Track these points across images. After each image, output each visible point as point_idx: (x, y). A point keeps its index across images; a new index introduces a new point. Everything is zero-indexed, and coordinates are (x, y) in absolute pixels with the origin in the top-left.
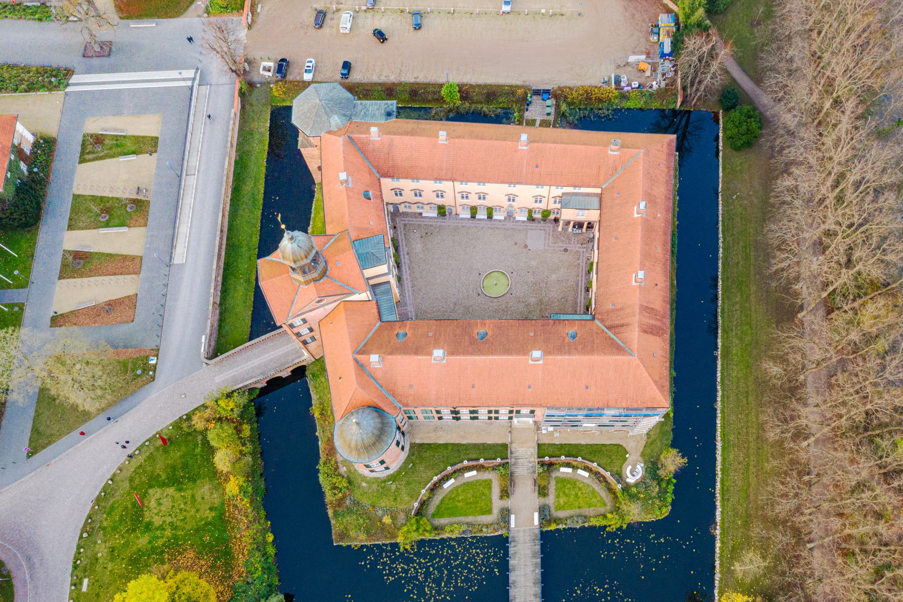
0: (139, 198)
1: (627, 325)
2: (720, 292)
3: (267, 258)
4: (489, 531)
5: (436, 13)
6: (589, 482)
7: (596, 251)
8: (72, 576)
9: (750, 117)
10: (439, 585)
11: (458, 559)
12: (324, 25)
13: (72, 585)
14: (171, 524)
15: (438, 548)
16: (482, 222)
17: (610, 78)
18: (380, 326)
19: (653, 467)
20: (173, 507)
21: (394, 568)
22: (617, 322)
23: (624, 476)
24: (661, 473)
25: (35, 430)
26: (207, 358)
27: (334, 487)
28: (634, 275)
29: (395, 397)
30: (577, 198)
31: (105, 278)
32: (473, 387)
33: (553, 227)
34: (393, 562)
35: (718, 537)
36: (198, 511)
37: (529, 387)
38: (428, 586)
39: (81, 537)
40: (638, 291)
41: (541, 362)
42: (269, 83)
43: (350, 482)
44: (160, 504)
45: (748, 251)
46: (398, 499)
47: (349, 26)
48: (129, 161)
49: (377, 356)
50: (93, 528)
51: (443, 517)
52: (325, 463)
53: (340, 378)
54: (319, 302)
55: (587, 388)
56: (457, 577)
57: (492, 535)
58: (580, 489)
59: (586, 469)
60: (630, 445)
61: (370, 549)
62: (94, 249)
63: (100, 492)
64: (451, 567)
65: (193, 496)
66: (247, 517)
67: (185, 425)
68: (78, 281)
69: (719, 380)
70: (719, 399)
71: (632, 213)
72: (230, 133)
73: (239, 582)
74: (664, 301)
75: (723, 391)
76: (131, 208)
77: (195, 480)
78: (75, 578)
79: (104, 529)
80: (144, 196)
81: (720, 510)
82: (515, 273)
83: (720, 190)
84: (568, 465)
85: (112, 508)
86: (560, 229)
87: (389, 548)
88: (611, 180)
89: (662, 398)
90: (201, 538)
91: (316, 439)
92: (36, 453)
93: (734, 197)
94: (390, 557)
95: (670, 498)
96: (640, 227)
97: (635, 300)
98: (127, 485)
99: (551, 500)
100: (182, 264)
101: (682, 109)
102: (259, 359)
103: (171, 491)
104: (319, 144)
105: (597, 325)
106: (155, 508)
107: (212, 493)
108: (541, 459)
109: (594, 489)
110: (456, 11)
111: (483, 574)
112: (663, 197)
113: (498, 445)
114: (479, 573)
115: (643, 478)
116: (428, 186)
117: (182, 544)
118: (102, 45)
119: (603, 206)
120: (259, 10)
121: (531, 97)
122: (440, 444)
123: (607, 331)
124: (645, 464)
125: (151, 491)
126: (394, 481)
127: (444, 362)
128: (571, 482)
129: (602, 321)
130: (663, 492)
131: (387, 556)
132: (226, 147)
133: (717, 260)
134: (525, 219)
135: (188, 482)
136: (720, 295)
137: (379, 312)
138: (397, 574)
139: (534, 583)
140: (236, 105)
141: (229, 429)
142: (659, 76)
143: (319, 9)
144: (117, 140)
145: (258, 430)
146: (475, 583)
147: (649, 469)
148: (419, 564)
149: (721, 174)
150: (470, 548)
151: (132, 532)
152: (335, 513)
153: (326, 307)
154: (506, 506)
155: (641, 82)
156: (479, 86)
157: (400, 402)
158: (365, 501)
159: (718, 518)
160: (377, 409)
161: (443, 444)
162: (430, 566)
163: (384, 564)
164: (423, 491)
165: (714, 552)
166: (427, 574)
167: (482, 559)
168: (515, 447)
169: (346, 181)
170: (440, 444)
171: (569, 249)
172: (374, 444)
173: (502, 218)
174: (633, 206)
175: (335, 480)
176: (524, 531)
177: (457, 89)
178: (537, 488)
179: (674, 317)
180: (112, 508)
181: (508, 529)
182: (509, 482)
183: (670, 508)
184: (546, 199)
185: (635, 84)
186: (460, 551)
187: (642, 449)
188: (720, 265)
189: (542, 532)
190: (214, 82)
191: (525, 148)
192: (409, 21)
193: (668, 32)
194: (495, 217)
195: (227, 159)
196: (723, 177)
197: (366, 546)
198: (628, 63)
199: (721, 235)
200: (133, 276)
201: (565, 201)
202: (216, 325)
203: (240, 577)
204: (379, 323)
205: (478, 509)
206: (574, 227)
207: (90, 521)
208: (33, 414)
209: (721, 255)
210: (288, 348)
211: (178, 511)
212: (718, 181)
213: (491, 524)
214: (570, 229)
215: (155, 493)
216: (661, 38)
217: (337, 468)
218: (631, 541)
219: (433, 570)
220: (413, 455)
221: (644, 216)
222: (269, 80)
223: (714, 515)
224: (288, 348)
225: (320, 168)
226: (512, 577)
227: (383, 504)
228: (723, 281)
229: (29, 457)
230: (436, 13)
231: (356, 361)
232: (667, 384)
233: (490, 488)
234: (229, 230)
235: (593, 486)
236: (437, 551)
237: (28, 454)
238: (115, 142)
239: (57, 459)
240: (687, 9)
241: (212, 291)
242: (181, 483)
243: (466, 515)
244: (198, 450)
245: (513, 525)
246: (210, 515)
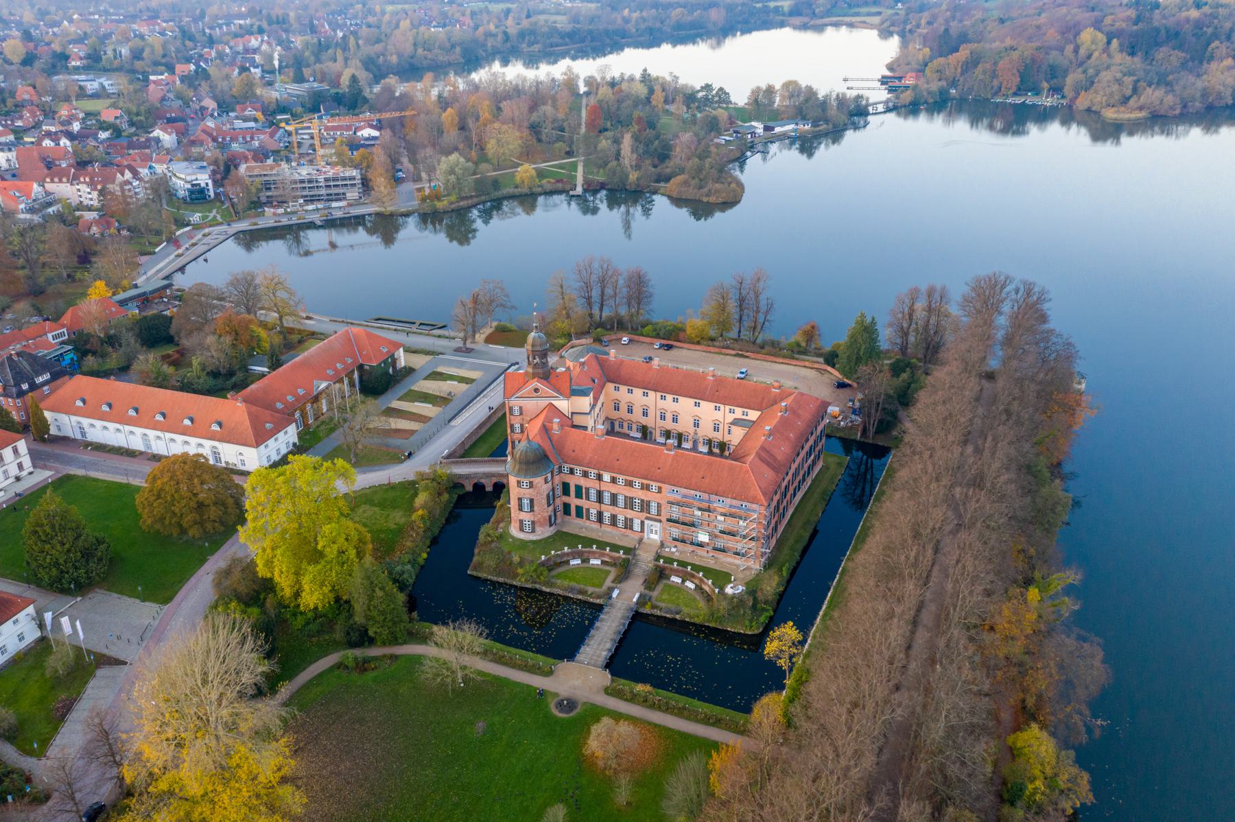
114: (572, 620)
128: (679, 589)
168: (638, 552)
172: (533, 463)
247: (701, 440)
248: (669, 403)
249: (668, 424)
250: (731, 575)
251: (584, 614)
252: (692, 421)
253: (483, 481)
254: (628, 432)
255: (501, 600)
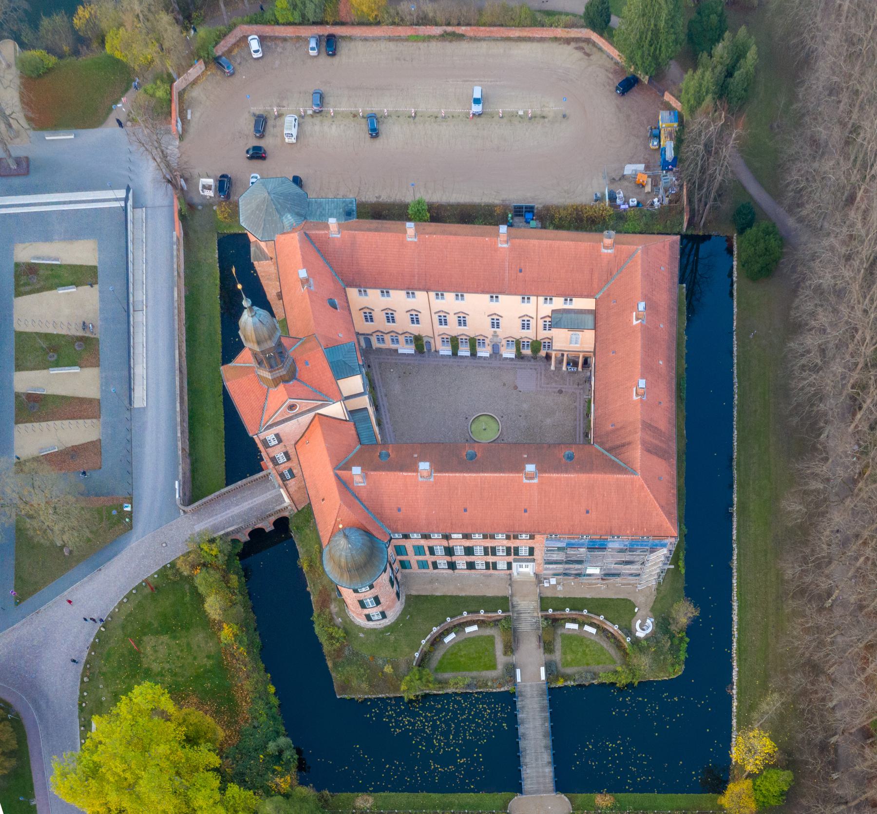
0: (86, 335)
1: (629, 443)
2: (735, 444)
3: (230, 365)
4: (495, 686)
5: (394, 117)
6: (596, 639)
7: (593, 378)
8: (80, 718)
9: (768, 233)
10: (447, 738)
11: (465, 714)
12: (267, 134)
13: (81, 726)
14: (170, 671)
15: (444, 702)
16: (466, 360)
17: (603, 195)
18: (360, 449)
19: (664, 623)
20: (169, 654)
21: (400, 721)
22: (618, 443)
23: (633, 631)
24: (673, 628)
25: (19, 578)
26: (184, 505)
27: (331, 637)
28: (635, 389)
29: (383, 522)
30: (569, 316)
31: (64, 422)
32: (465, 510)
33: (545, 365)
34: (399, 714)
35: (735, 697)
36: (195, 658)
37: (526, 511)
38: (436, 739)
39: (82, 682)
40: (639, 407)
41: (536, 481)
42: (212, 205)
43: (346, 632)
44: (156, 651)
45: (767, 397)
46: (398, 650)
47: (294, 132)
48: (68, 294)
49: (335, 219)
50: (93, 674)
51: (446, 672)
52: (319, 616)
53: (323, 500)
54: (292, 407)
55: (587, 512)
56: (465, 730)
57: (498, 690)
58: (587, 646)
59: (592, 625)
60: (640, 600)
61: (375, 702)
62: (49, 391)
63: (94, 639)
64: (458, 720)
65: (188, 644)
66: (245, 666)
67: (170, 572)
68: (36, 425)
69: (734, 538)
70: (735, 557)
71: (631, 321)
72: (175, 260)
73: (245, 726)
74: (670, 423)
75: (739, 548)
76: (80, 346)
77: (188, 629)
78: (83, 719)
79: (104, 674)
80: (92, 333)
81: (737, 669)
82: (505, 417)
83: (734, 328)
84: (574, 621)
85: (109, 655)
86: (553, 368)
87: (393, 702)
88: (605, 289)
89: (669, 525)
90: (202, 685)
91: (308, 594)
92: (24, 600)
93: (751, 337)
94: (395, 711)
95: (683, 656)
96: (640, 334)
97: (636, 416)
98: (119, 632)
99: (557, 656)
100: (144, 408)
101: (689, 233)
102: (237, 507)
103: (165, 638)
104: (273, 256)
105: (596, 449)
106: (152, 655)
107: (207, 642)
108: (545, 613)
109: (602, 646)
110: (418, 115)
111: (491, 728)
112: (666, 306)
113: (498, 598)
114: (487, 727)
115: (653, 633)
116: (398, 300)
117: (183, 690)
118: (18, 161)
119: (599, 324)
120: (189, 117)
121: (512, 218)
122: (437, 596)
123: (608, 454)
124: (655, 619)
125: (145, 638)
126: (392, 632)
127: (432, 480)
128: (579, 639)
129: (602, 444)
130: (674, 649)
131: (391, 710)
132: (173, 277)
133: (732, 407)
134: (513, 356)
135: (181, 630)
136: (735, 447)
137: (358, 435)
138: (404, 726)
139: (544, 736)
140: (177, 228)
141: (215, 576)
142: (661, 191)
143: (257, 113)
144: (52, 270)
145: (246, 585)
146: (484, 737)
147: (660, 624)
148: (426, 717)
149: (735, 310)
150: (477, 703)
151: (132, 677)
152: (335, 665)
153: (300, 419)
154: (511, 661)
155: (640, 200)
156: (452, 206)
157: (389, 527)
158: (365, 652)
159: (735, 678)
160: (367, 532)
161: (441, 596)
162: (437, 719)
163: (390, 717)
164: (423, 642)
165: (731, 711)
166: (435, 727)
167: (489, 714)
168: (516, 600)
169: (307, 280)
170: (437, 596)
171: (563, 390)
172: (365, 565)
173: (487, 355)
174: (632, 312)
175: (331, 630)
176: (531, 686)
177: (426, 207)
178: (542, 644)
179: (684, 469)
180: (109, 655)
181: (515, 683)
182: (512, 637)
183: (683, 667)
184: (535, 320)
185: (633, 202)
186: (466, 706)
187: (652, 604)
188: (735, 413)
189: (550, 689)
190: (149, 203)
191: (505, 246)
192: (364, 127)
193: (670, 134)
194: (479, 354)
195: (176, 289)
196: (738, 313)
197: (370, 700)
198: (624, 176)
199: (736, 380)
200: (94, 420)
201: (556, 320)
202: (188, 474)
203: (246, 722)
204: (359, 447)
205: (482, 664)
206: (568, 364)
207: (88, 666)
208: (13, 562)
209: (736, 402)
210: (268, 496)
211: (175, 658)
212: (733, 318)
213: (497, 679)
214: (564, 368)
215: (149, 643)
216: (662, 143)
217: (332, 619)
218: (644, 699)
219: (441, 723)
220: (410, 606)
221: (644, 323)
222: (211, 201)
223: (731, 675)
224: (268, 496)
225: (280, 296)
226: (521, 730)
227: (383, 655)
228: (738, 431)
229: (17, 604)
230: (394, 117)
231: (338, 477)
232: (675, 512)
233: (493, 644)
234: (188, 374)
235: (602, 643)
236: (443, 706)
237: (16, 602)
238: (50, 272)
239: (46, 606)
240: (692, 102)
241: (179, 435)
242: (175, 631)
243: (470, 670)
244: (187, 599)
245: (519, 680)
246: (209, 663)
247: (504, 342)
248: (449, 302)
249: (453, 330)
250: (635, 607)
251: (496, 715)
252: (488, 321)
253: (259, 526)
254: (394, 346)
255: (397, 726)
